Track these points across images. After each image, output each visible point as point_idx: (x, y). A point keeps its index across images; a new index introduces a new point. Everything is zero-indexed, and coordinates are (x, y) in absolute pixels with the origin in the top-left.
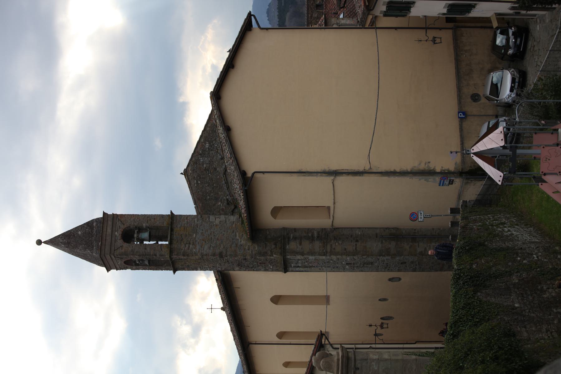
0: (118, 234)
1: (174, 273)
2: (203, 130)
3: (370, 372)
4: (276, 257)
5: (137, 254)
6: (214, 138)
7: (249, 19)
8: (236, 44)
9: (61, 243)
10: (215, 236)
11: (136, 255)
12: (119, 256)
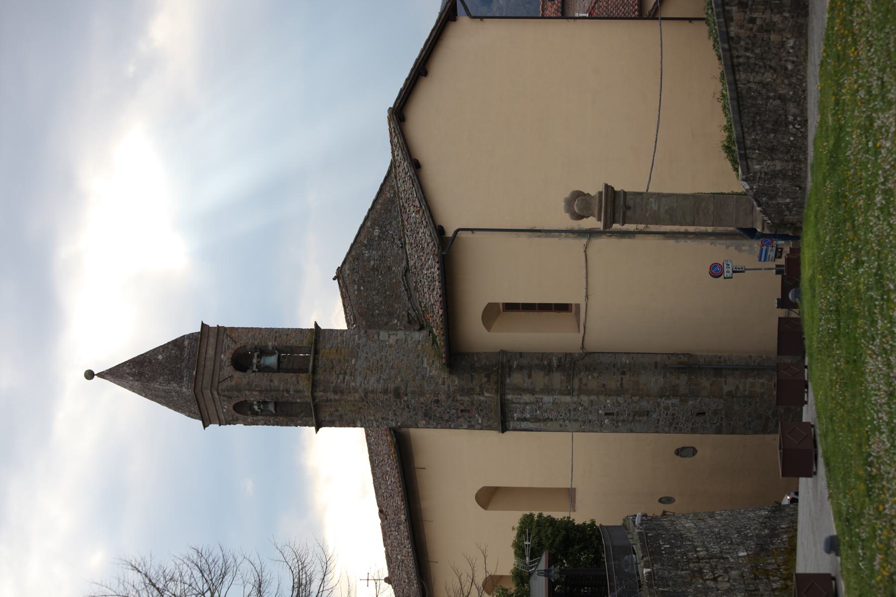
0: (225, 357)
1: (317, 430)
2: (369, 207)
3: (647, 214)
4: (489, 396)
5: (257, 389)
6: (389, 221)
7: (452, 2)
8: (432, 38)
9: (128, 374)
10: (387, 362)
11: (256, 391)
12: (226, 393)
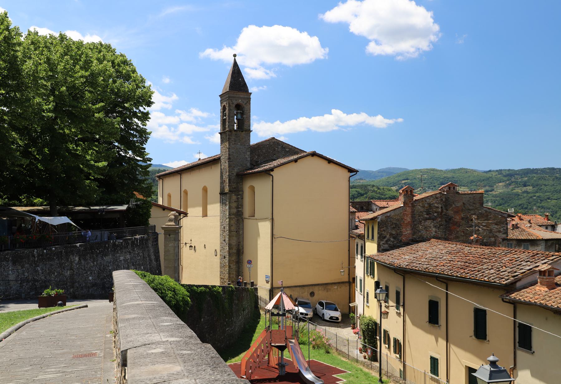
1: (219, 133)
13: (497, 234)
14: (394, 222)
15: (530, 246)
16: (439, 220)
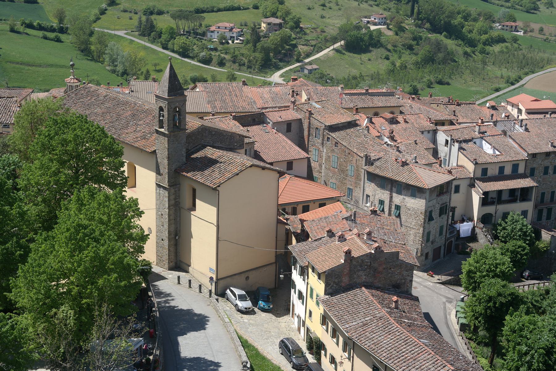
13: (407, 277)
14: (337, 274)
15: (417, 193)
16: (368, 270)
